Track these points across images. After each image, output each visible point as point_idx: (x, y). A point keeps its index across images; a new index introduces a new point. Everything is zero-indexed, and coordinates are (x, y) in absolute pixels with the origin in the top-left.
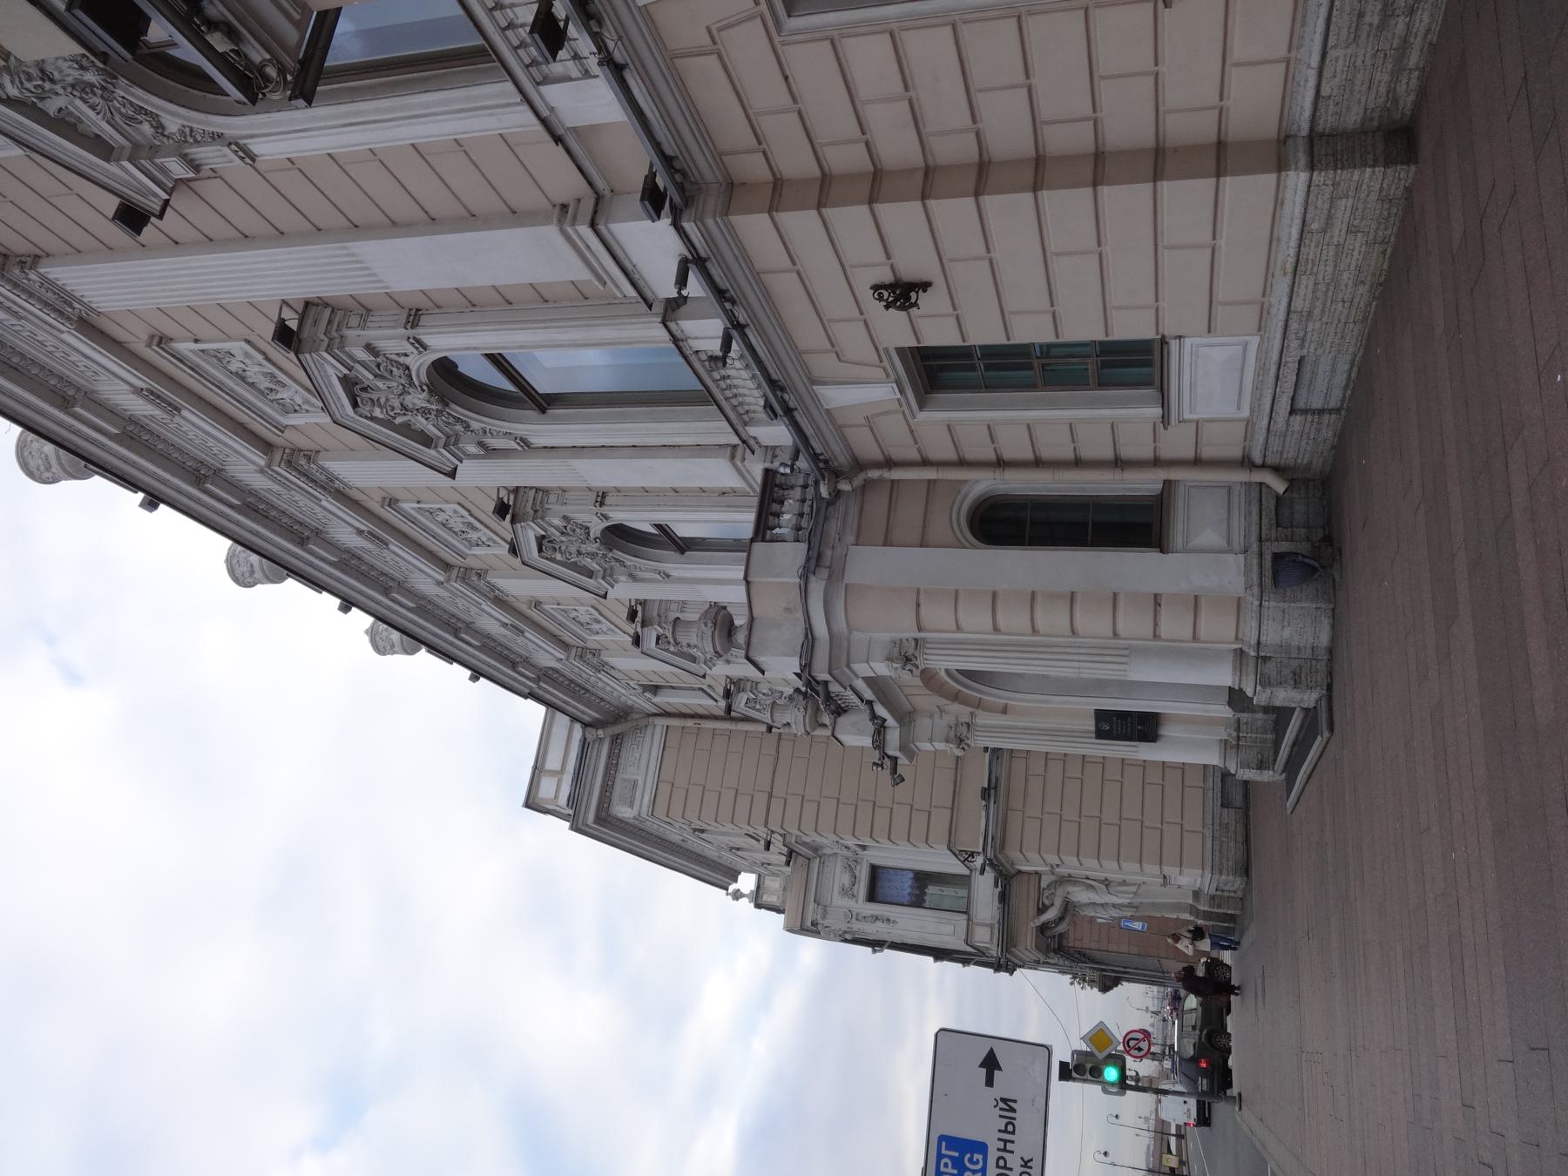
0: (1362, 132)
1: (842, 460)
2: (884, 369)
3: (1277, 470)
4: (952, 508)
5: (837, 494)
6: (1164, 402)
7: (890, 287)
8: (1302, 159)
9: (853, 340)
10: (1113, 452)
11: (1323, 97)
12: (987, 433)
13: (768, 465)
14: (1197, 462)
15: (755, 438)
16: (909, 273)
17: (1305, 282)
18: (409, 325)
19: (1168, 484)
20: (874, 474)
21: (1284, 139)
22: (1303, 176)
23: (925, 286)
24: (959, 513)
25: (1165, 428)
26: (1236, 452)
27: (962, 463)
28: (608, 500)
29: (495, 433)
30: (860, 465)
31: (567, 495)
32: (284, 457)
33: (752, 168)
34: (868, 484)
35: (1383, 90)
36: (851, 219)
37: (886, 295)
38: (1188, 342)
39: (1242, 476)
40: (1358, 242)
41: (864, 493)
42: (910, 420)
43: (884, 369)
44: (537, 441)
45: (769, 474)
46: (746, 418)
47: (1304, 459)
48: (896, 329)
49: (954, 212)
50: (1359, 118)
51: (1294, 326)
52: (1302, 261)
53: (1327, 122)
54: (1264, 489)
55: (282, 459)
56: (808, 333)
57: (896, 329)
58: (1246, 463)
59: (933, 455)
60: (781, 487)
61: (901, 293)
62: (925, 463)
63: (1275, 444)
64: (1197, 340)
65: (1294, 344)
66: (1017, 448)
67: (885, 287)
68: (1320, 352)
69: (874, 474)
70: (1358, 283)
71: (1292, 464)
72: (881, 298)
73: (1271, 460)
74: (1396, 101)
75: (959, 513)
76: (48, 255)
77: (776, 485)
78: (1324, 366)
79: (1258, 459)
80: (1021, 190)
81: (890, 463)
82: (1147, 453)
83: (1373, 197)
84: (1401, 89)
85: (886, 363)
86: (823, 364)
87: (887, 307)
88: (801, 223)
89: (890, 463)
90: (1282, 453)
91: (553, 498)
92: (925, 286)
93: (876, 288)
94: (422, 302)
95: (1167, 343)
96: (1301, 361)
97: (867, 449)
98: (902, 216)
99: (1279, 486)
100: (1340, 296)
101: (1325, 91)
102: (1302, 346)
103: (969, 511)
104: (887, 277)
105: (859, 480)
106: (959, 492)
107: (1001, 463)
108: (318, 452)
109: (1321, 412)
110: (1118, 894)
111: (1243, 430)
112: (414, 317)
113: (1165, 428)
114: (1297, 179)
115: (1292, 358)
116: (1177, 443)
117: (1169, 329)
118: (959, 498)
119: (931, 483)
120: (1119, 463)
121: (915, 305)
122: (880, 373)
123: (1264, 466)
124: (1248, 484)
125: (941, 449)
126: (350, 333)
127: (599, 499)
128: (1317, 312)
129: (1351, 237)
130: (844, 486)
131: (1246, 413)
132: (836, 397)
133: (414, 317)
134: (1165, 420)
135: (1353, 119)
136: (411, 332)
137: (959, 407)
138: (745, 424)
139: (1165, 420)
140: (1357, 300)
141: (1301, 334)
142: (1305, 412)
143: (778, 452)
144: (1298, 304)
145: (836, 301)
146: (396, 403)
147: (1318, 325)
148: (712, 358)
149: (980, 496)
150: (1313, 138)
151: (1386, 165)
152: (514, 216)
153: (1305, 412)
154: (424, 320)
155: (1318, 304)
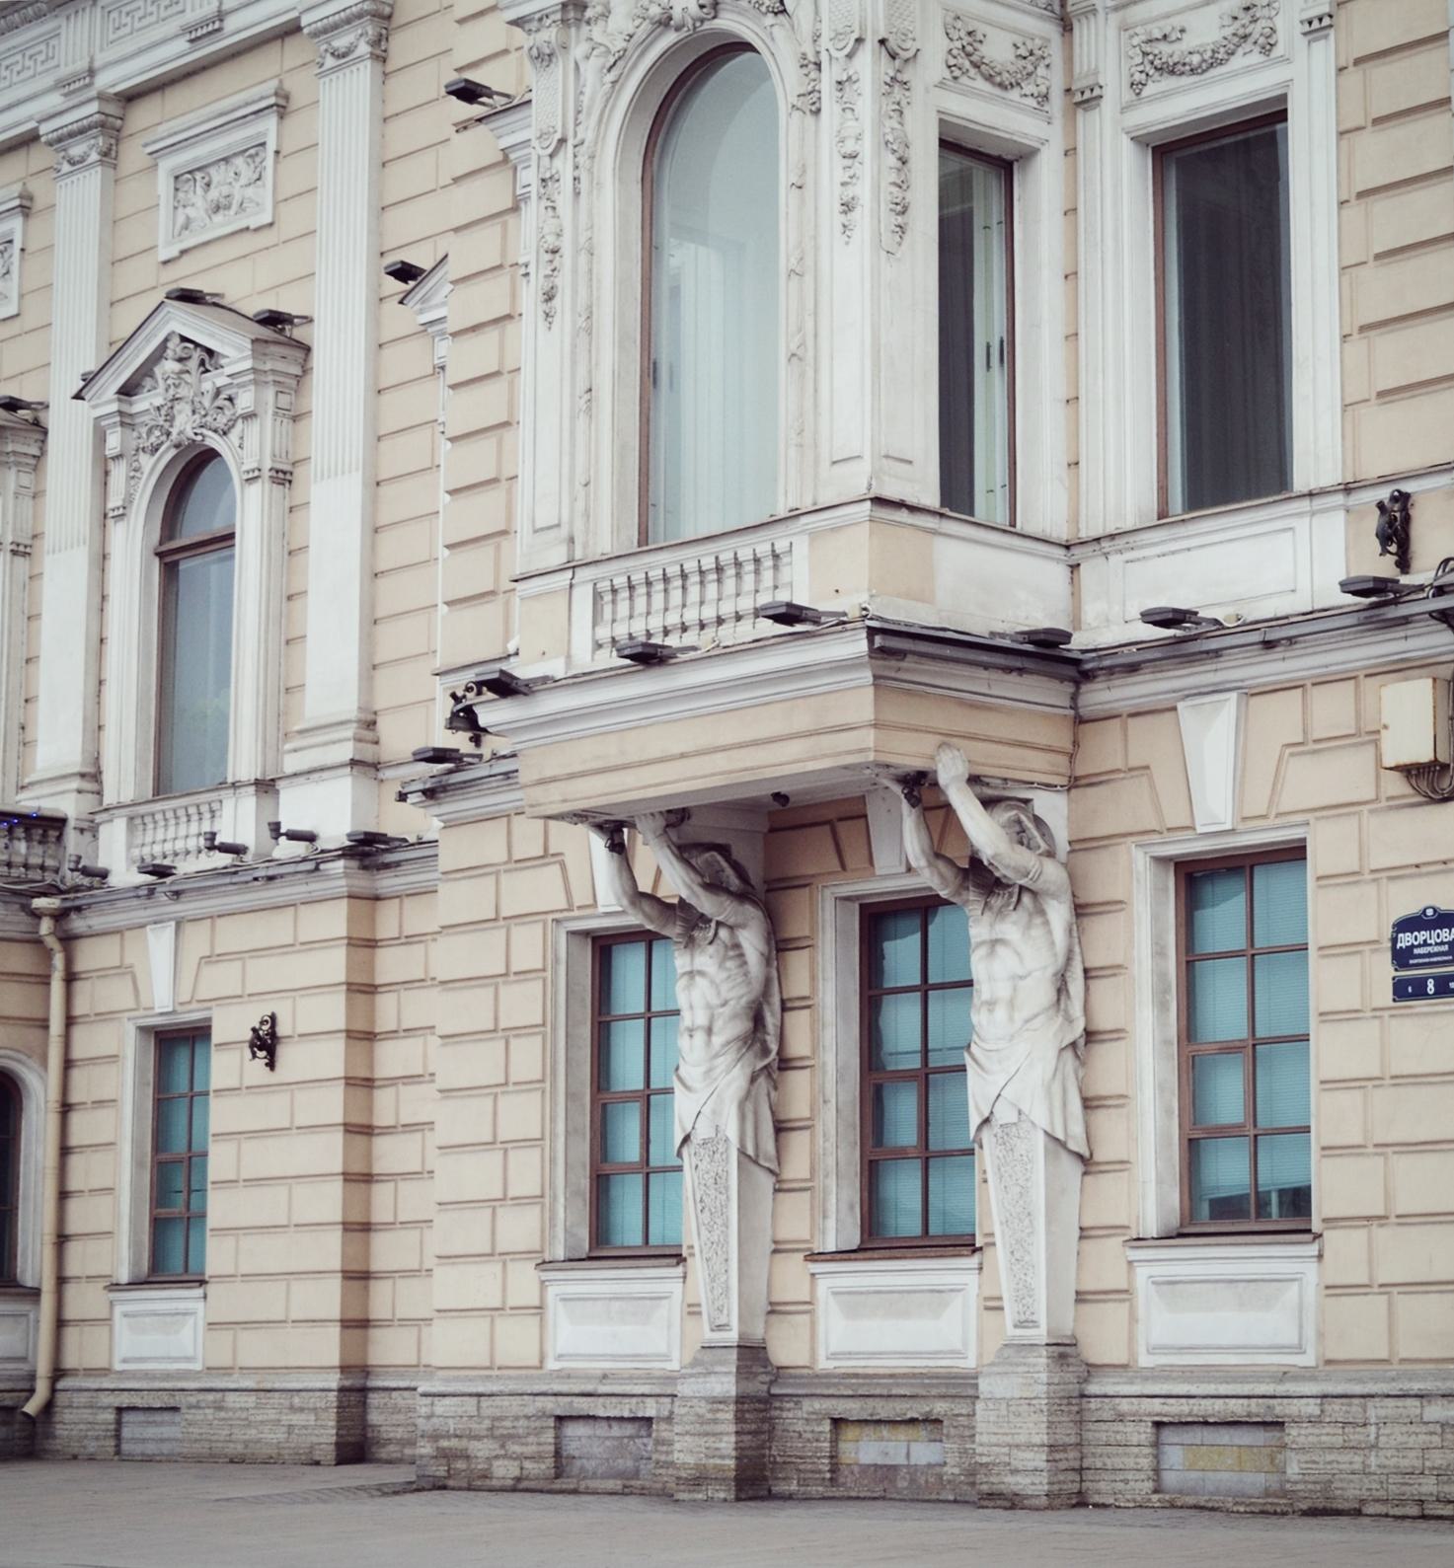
0: (364, 1425)
1: (77, 924)
2: (189, 1002)
3: (49, 1407)
4: (11, 1049)
5: (37, 915)
6: (136, 1284)
7: (273, 1034)
8: (347, 1383)
9: (222, 980)
10: (79, 1232)
11: (432, 1404)
12: (106, 1097)
13: (71, 823)
14: (60, 1323)
15: (111, 821)
16: (283, 1052)
17: (250, 1400)
18: (274, 474)
19: (35, 1294)
20: (58, 960)
21: (365, 1370)
22: (334, 1385)
23: (271, 1065)
24: (9, 1058)
25: (105, 1288)
26: (70, 1361)
27: (68, 1064)
28: (19, 560)
29: (132, 482)
30: (68, 940)
31: (28, 502)
32: (111, 119)
33: (388, 920)
34: (48, 954)
35: (392, 1435)
36: (332, 1012)
37: (266, 1027)
38: (200, 1306)
39: (43, 1368)
40: (280, 1435)
41: (28, 941)
42: (127, 1014)
43: (189, 1002)
44: (118, 533)
45: (58, 823)
46: (138, 821)
47: (60, 1431)
48: (232, 1026)
49: (332, 1105)
50: (375, 1422)
51: (210, 1397)
52: (269, 1395)
53: (374, 1399)
54: (24, 1394)
55: (107, 115)
56: (235, 934)
57: (232, 1026)
58: (58, 1373)
59: (78, 1033)
60: (45, 835)
61: (266, 1043)
62: (70, 1021)
63: (81, 1399)
64: (201, 1314)
65: (193, 1400)
66: (81, 1128)
67: (273, 1026)
68: (184, 1423)
69: (58, 960)
70: (246, 1444)
71: (57, 1418)
72: (262, 1023)
73: (62, 1399)
74: (384, 1446)
75: (9, 1058)
76: (385, 74)
77: (45, 831)
78: (167, 1431)
79: (60, 1385)
80: (345, 1162)
81: (70, 978)
82: (72, 1268)
83: (315, 1440)
84: (391, 1448)
85: (195, 1006)
86: (198, 939)
87: (254, 1030)
88: (334, 965)
89: (70, 978)
90: (70, 1407)
91: (26, 479)
92: (271, 1065)
93: (273, 1018)
94: (298, 494)
95: (678, 1264)
96: (175, 1409)
97: (89, 956)
98: (332, 1058)
99: (32, 1407)
100: (235, 1431)
101: (395, 1394)
102: (190, 1407)
103: (12, 1071)
104: (281, 1031)
105: (52, 942)
106: (29, 1057)
107: (66, 1108)
108: (115, 167)
109: (118, 1437)
110: (1059, 1076)
111: (801, 1364)
112: (283, 477)
113: (105, 1288)
114: (333, 1381)
115: (179, 1400)
116: (82, 1301)
117: (212, 1289)
118: (23, 1057)
119: (44, 1024)
120: (62, 1239)
121: (254, 1055)
122: (186, 997)
123: (53, 1391)
124: (32, 1377)
125: (85, 1043)
126: (269, 394)
127: (21, 549)
128: (223, 1414)
129: (284, 1429)
130: (46, 926)
131: (118, 1366)
132: (159, 943)
133: (283, 477)
134: (115, 1287)
135: (374, 1417)
136: (266, 474)
137: (139, 1069)
138: (131, 819)
139: (115, 1287)
140: (232, 1445)
141: (203, 1405)
142: (119, 1423)
143: (88, 835)
144: (231, 1397)
145: (266, 974)
146: (183, 392)
147: (211, 1417)
148: (213, 836)
149: (22, 1080)
150: (364, 1390)
151: (337, 1444)
152: (371, 668)
153: (119, 1423)
154: (277, 489)
155: (230, 1414)
